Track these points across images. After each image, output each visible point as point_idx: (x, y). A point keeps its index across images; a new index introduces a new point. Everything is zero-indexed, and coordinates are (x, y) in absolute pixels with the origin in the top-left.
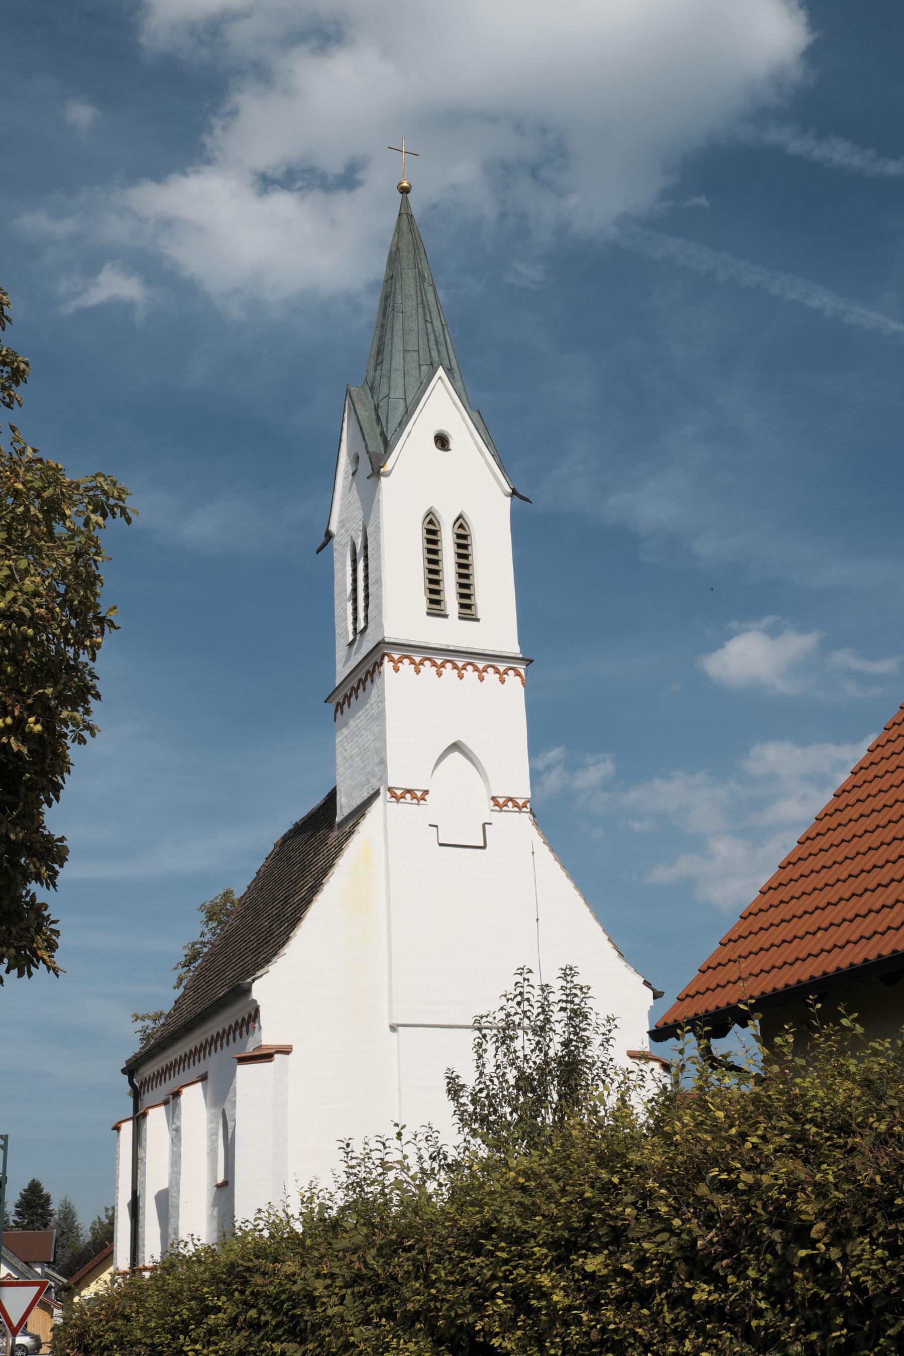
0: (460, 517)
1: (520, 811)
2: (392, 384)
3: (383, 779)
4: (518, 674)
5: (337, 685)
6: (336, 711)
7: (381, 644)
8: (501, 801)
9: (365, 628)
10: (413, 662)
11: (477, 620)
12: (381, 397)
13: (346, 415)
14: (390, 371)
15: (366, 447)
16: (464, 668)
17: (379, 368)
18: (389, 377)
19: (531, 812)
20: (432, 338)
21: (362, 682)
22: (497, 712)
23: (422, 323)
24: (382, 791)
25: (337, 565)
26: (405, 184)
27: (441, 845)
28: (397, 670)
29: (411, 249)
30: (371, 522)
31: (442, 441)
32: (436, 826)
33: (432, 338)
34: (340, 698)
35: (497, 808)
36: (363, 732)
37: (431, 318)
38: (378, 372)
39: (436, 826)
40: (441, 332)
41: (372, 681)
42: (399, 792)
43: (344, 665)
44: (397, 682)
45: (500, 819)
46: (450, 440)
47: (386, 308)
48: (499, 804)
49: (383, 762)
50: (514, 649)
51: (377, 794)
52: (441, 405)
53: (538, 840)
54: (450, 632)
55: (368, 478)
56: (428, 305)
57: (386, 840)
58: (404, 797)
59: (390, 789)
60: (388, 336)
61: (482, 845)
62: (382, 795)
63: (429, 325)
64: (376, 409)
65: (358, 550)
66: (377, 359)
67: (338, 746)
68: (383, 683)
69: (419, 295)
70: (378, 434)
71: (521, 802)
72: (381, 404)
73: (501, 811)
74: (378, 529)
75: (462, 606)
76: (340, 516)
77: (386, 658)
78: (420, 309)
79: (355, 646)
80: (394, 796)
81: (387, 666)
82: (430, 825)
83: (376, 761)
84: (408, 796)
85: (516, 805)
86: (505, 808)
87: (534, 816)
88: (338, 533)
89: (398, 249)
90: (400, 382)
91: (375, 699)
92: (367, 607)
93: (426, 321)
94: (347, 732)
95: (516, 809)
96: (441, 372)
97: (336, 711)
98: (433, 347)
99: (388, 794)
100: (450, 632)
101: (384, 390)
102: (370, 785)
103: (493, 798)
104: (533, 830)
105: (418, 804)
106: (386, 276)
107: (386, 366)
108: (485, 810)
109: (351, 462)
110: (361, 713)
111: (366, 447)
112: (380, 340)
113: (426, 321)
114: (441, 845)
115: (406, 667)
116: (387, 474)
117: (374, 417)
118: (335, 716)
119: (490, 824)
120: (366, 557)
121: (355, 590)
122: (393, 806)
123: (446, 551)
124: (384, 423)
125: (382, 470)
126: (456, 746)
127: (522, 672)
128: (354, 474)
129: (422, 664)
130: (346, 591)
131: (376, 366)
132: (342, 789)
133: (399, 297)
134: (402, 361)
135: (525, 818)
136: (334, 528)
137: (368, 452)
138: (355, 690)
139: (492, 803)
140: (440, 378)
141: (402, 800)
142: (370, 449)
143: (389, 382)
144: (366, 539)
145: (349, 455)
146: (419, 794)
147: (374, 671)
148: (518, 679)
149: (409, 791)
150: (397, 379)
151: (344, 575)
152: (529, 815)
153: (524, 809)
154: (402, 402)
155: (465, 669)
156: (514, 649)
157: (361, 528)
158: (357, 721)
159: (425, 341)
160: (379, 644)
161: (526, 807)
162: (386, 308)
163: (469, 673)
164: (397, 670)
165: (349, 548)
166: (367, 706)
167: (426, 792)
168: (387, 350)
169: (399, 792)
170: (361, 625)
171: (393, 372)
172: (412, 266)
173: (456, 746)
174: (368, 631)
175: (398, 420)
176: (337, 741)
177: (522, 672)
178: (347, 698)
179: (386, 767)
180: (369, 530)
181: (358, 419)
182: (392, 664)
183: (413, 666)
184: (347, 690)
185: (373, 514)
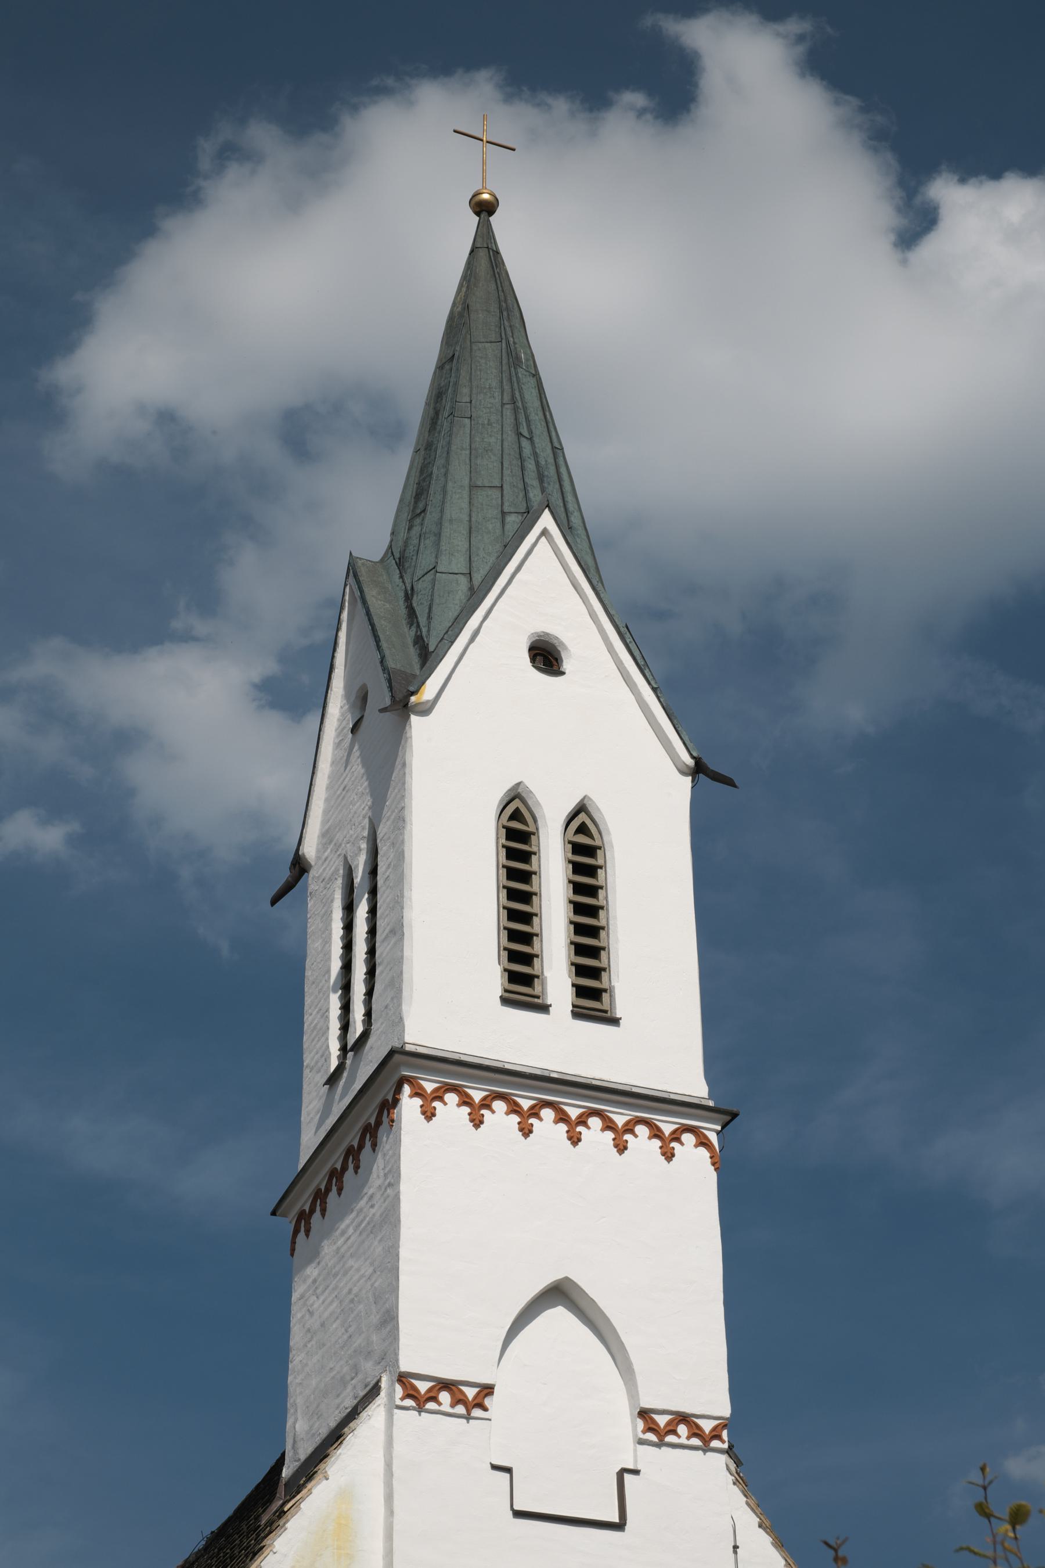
0: (581, 809)
1: (706, 1448)
2: (444, 546)
3: (389, 1355)
4: (703, 1142)
5: (300, 1166)
6: (296, 1232)
7: (396, 1054)
8: (662, 1420)
9: (365, 1035)
10: (466, 1101)
11: (615, 1021)
12: (419, 573)
13: (345, 615)
14: (440, 523)
15: (382, 661)
17: (418, 521)
18: (438, 535)
19: (730, 1452)
20: (530, 465)
21: (353, 1154)
22: (659, 1231)
23: (510, 437)
24: (384, 1384)
25: (313, 925)
26: (486, 196)
27: (519, 1514)
28: (429, 1114)
29: (494, 308)
30: (387, 813)
31: (546, 656)
33: (530, 465)
34: (304, 1202)
35: (651, 1437)
36: (351, 1262)
37: (530, 432)
38: (416, 530)
39: (508, 1470)
40: (551, 460)
41: (374, 1146)
42: (423, 1387)
43: (316, 1132)
45: (655, 1461)
46: (563, 655)
47: (437, 413)
48: (658, 1427)
49: (389, 1320)
50: (695, 1086)
51: (374, 1391)
53: (748, 1520)
54: (552, 1040)
55: (382, 711)
56: (525, 409)
57: (389, 1498)
58: (434, 1399)
59: (403, 1378)
60: (440, 462)
61: (616, 1519)
62: (383, 1394)
63: (525, 443)
64: (408, 597)
65: (357, 881)
66: (415, 508)
67: (294, 1308)
68: (398, 1142)
69: (507, 387)
70: (410, 641)
71: (707, 1426)
72: (418, 586)
73: (661, 1444)
74: (401, 821)
75: (581, 992)
76: (324, 822)
77: (407, 1089)
78: (508, 411)
79: (342, 1083)
80: (411, 1393)
81: (409, 1106)
82: (495, 1467)
83: (375, 1319)
84: (445, 1397)
85: (696, 1432)
86: (670, 1439)
87: (738, 1463)
88: (318, 858)
89: (467, 307)
90: (461, 543)
91: (378, 1182)
92: (369, 993)
93: (519, 435)
94: (316, 1273)
95: (696, 1442)
96: (546, 520)
97: (296, 1232)
98: (532, 481)
99: (399, 1391)
100: (552, 1040)
101: (425, 560)
102: (360, 1376)
104: (736, 1498)
105: (468, 1417)
106: (440, 359)
107: (431, 516)
109: (352, 707)
110: (347, 1221)
111: (382, 661)
112: (422, 472)
113: (519, 435)
114: (519, 1514)
115: (451, 1111)
116: (425, 710)
117: (403, 611)
118: (293, 1243)
119: (636, 1472)
120: (373, 892)
121: (347, 967)
122: (408, 1420)
123: (549, 889)
124: (422, 620)
125: (413, 699)
126: (560, 1293)
127: (713, 1137)
128: (354, 729)
129: (488, 1107)
130: (328, 971)
131: (411, 520)
132: (300, 1401)
133: (465, 391)
134: (465, 505)
135: (716, 1465)
136: (310, 850)
137: (385, 669)
138: (336, 1176)
139: (640, 1424)
140: (545, 533)
141: (431, 1405)
142: (391, 664)
143: (437, 544)
144: (374, 853)
145: (347, 695)
146: (470, 1393)
147: (379, 1123)
148: (704, 1153)
149: (446, 1385)
150: (455, 539)
151: (327, 941)
152: (723, 1458)
153: (715, 1444)
154: (463, 581)
155: (584, 1123)
156: (695, 1086)
157: (366, 833)
158: (339, 1241)
159: (517, 471)
160: (392, 1053)
161: (719, 1437)
162: (437, 413)
163: (594, 1133)
164: (429, 1114)
165: (339, 882)
166: (362, 1203)
167: (487, 1390)
168: (435, 487)
169: (423, 1387)
170: (358, 1028)
171: (446, 524)
172: (493, 337)
173: (560, 1293)
174: (371, 1041)
175: (452, 614)
176: (295, 1296)
177: (713, 1137)
178: (320, 1197)
179: (396, 1328)
180: (381, 831)
181: (368, 613)
182: (418, 1102)
183: (466, 1110)
184: (319, 1180)
185: (392, 794)
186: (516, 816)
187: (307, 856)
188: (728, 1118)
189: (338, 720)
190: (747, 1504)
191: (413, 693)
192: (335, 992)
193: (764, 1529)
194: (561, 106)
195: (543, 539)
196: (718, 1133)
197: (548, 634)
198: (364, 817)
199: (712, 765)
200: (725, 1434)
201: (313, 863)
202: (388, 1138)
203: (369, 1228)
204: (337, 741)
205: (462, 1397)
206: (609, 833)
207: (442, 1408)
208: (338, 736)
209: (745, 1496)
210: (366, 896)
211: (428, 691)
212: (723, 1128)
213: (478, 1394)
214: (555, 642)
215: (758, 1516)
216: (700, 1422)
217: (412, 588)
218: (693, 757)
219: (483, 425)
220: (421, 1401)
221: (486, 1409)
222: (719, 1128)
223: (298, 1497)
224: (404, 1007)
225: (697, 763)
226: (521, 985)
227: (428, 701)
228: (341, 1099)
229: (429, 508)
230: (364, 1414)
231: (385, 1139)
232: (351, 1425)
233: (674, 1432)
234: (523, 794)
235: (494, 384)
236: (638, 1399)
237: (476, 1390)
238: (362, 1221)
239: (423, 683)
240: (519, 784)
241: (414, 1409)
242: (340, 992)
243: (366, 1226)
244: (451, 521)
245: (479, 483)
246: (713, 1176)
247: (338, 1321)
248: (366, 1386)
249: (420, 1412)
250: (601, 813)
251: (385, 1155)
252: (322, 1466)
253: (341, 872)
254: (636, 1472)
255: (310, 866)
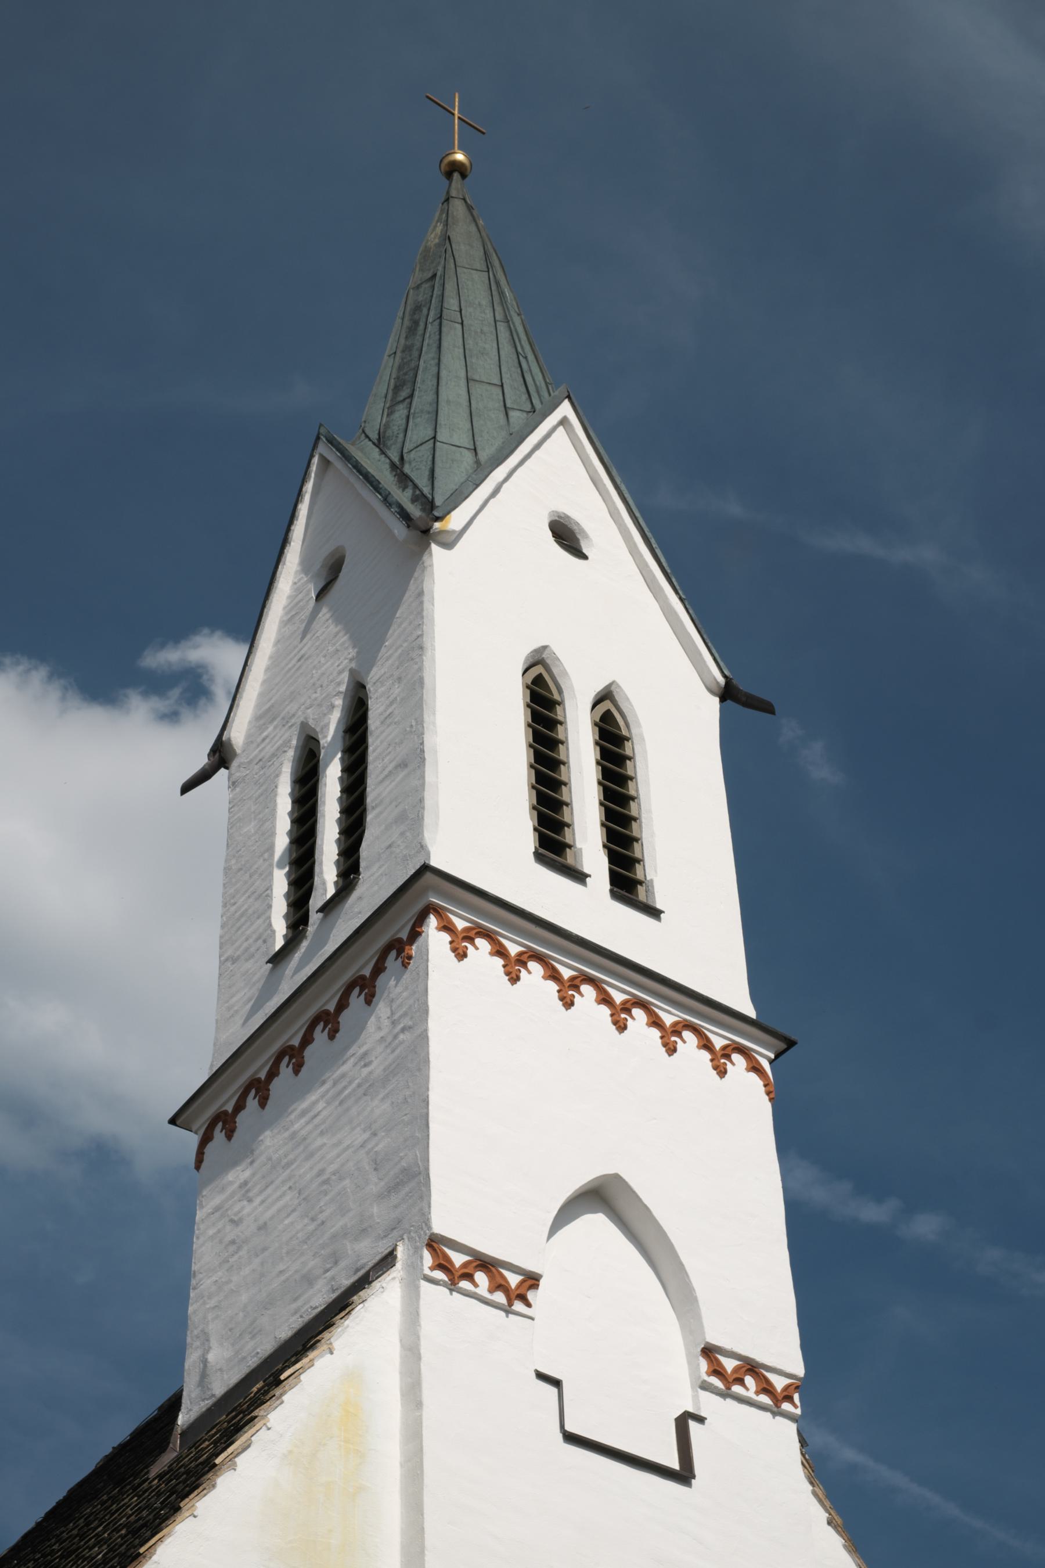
1: (777, 1412)
4: (755, 1068)
13: (309, 487)
16: (626, 1008)
22: (716, 1147)
24: (400, 1252)
27: (571, 1438)
31: (566, 536)
32: (556, 1383)
39: (556, 1383)
44: (458, 985)
51: (388, 1261)
52: (557, 468)
58: (469, 1277)
59: (435, 1243)
62: (399, 1265)
77: (433, 921)
78: (502, 327)
80: (444, 1265)
81: (436, 940)
82: (541, 1376)
84: (481, 1277)
94: (247, 1173)
95: (764, 1399)
99: (428, 1259)
103: (709, 1352)
105: (508, 1310)
108: (679, 1385)
110: (313, 1097)
114: (571, 1438)
116: (449, 542)
119: (701, 1420)
123: (577, 767)
125: (437, 525)
126: (601, 1196)
127: (766, 1065)
130: (271, 848)
132: (214, 1328)
139: (703, 1365)
141: (464, 1284)
145: (305, 564)
149: (486, 1264)
153: (786, 1406)
154: (468, 457)
167: (532, 1280)
177: (766, 1065)
182: (446, 937)
186: (539, 680)
187: (234, 742)
188: (783, 1046)
189: (289, 597)
190: (814, 1493)
191: (438, 519)
192: (280, 866)
193: (835, 1528)
194: (39, 675)
195: (561, 428)
196: (771, 1062)
197: (568, 517)
198: (340, 672)
199: (743, 685)
200: (796, 1397)
201: (238, 751)
202: (398, 981)
203: (361, 1091)
204: (285, 618)
205: (503, 1283)
206: (639, 726)
207: (478, 1291)
208: (287, 614)
209: (811, 1483)
210: (339, 755)
211: (455, 520)
212: (777, 1056)
213: (522, 1282)
214: (575, 528)
215: (827, 1511)
216: (772, 1377)
217: (402, 458)
218: (725, 676)
219: (476, 332)
220: (455, 1277)
221: (528, 1305)
222: (772, 1056)
223: (298, 1366)
224: (428, 836)
225: (727, 684)
226: (552, 845)
227: (454, 532)
228: (297, 971)
229: (416, 393)
230: (376, 1284)
231: (392, 982)
232: (361, 1293)
233: (741, 1381)
234: (548, 661)
235: (484, 303)
236: (703, 1333)
237: (520, 1278)
238: (345, 1088)
239: (449, 513)
240: (545, 647)
241: (445, 1285)
242: (287, 869)
243: (354, 1090)
244: (448, 402)
245: (477, 378)
246: (767, 1107)
247: (295, 1214)
248: (357, 1270)
249: (451, 1290)
250: (630, 703)
251: (392, 1001)
252: (326, 1335)
253: (294, 742)
254: (701, 1420)
255: (234, 754)
